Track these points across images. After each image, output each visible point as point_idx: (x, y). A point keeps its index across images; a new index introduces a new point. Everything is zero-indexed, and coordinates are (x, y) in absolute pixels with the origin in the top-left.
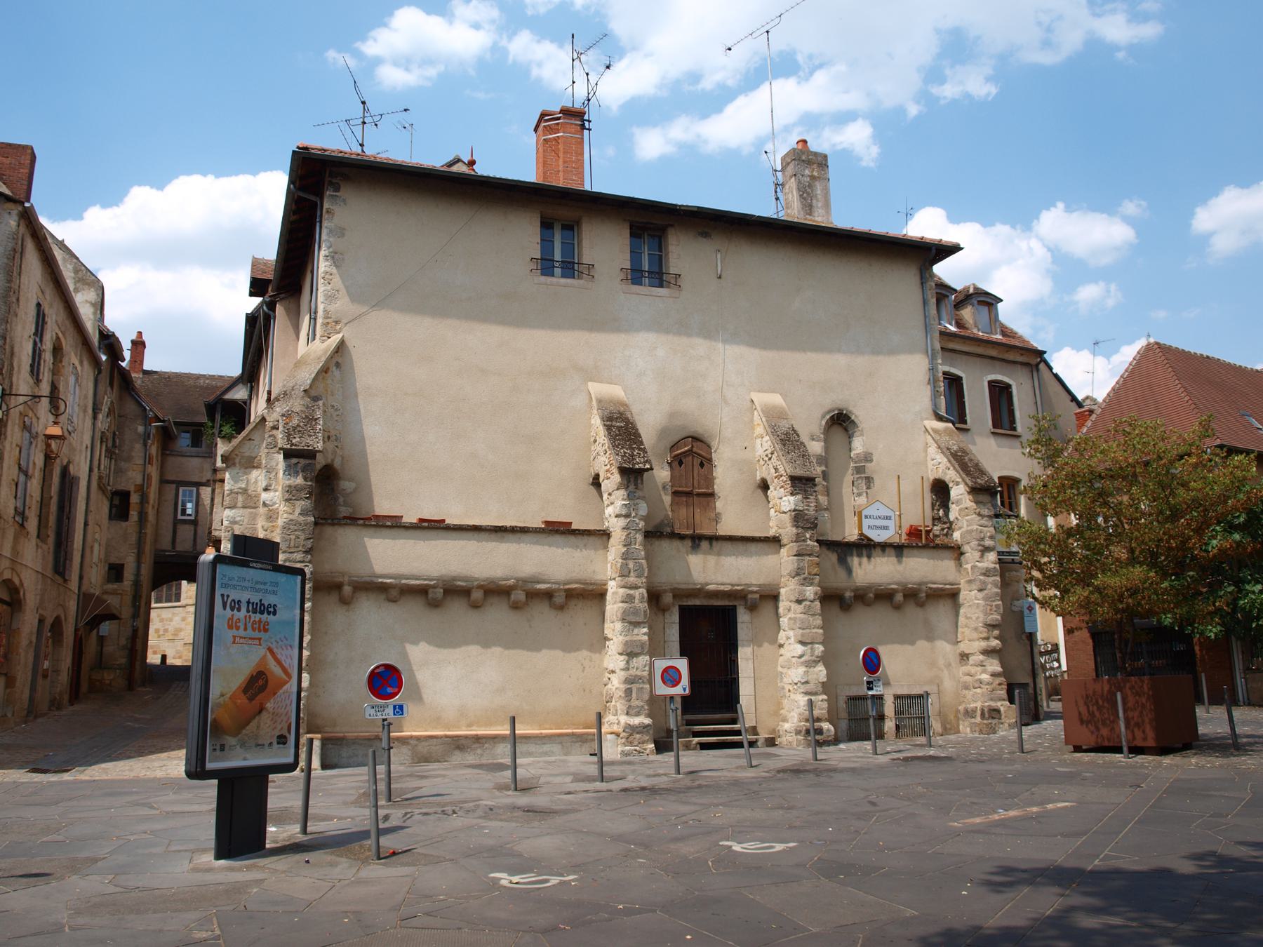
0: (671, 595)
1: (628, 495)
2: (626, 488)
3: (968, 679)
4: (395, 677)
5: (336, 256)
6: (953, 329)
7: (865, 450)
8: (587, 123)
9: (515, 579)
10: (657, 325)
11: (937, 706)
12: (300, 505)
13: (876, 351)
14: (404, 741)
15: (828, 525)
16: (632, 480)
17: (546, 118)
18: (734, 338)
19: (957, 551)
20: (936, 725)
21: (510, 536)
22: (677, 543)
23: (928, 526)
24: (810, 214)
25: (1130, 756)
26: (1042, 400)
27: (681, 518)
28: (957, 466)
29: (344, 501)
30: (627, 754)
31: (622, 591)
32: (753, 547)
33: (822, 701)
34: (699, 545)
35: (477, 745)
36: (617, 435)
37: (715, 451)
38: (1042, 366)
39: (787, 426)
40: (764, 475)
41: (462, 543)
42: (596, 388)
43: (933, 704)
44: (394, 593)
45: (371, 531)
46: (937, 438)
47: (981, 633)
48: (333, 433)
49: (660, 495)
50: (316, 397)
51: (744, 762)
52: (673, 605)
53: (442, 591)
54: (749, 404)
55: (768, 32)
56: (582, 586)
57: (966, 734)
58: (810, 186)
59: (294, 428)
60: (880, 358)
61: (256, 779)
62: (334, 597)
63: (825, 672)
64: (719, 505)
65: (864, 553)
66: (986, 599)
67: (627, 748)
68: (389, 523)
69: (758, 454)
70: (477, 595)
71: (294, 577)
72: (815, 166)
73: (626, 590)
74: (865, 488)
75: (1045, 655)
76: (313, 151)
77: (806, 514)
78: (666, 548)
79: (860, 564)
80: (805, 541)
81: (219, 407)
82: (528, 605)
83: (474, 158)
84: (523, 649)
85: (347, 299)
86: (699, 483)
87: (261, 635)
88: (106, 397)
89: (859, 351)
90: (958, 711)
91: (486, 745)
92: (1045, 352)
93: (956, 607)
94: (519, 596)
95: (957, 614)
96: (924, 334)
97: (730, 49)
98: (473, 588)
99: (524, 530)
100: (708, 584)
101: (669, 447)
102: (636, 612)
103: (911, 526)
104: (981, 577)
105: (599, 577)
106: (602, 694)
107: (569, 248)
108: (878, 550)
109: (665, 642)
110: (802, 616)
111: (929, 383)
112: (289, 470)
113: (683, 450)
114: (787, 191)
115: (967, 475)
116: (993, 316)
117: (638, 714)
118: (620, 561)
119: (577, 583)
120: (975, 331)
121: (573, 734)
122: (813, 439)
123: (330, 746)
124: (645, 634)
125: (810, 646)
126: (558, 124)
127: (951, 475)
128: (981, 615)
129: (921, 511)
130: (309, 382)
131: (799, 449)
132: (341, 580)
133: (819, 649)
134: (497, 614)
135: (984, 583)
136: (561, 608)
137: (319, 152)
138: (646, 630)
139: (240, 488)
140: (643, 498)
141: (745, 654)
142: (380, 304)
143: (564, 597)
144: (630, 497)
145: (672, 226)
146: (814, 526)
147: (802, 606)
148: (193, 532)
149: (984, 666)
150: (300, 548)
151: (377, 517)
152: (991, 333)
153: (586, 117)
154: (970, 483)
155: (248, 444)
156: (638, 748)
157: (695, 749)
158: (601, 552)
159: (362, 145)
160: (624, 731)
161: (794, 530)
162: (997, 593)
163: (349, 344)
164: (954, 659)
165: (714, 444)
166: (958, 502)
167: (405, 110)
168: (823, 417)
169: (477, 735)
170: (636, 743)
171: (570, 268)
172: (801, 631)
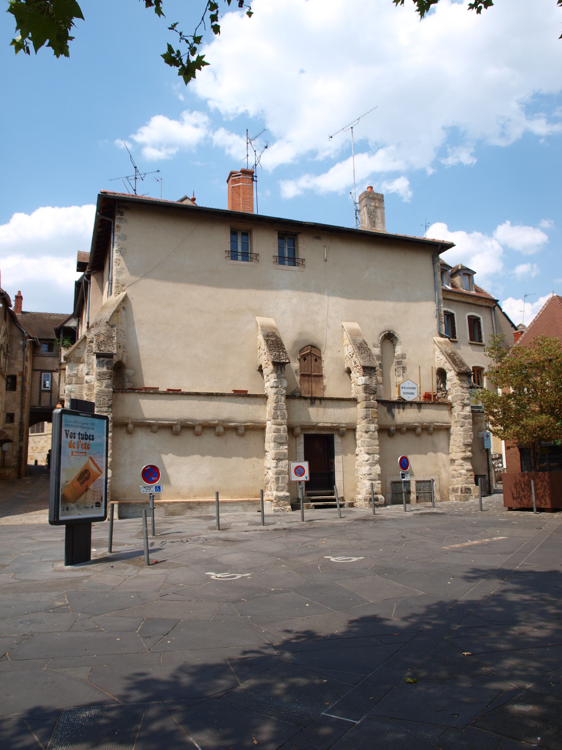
0: (300, 428)
1: (277, 376)
2: (276, 373)
3: (454, 472)
4: (156, 472)
5: (122, 250)
6: (449, 288)
7: (402, 353)
8: (255, 178)
9: (218, 420)
10: (293, 286)
11: (438, 487)
12: (105, 382)
13: (409, 300)
14: (161, 504)
15: (382, 392)
16: (279, 368)
17: (233, 175)
18: (333, 293)
19: (450, 406)
20: (437, 496)
21: (216, 398)
22: (303, 402)
23: (435, 393)
24: (374, 227)
25: (537, 513)
26: (497, 326)
27: (305, 388)
28: (450, 361)
29: (128, 380)
30: (277, 511)
31: (274, 426)
32: (342, 403)
33: (378, 484)
34: (314, 403)
35: (199, 507)
36: (271, 345)
37: (323, 353)
38: (496, 308)
39: (361, 340)
40: (349, 366)
41: (190, 402)
42: (260, 320)
43: (436, 486)
44: (155, 428)
45: (143, 396)
46: (440, 346)
47: (461, 449)
48: (122, 344)
49: (294, 376)
50: (113, 325)
51: (337, 515)
52: (301, 433)
53: (180, 427)
54: (341, 328)
55: (352, 128)
56: (253, 424)
57: (453, 501)
58: (374, 211)
59: (101, 342)
60: (411, 304)
61: (86, 524)
62: (124, 430)
63: (380, 469)
64: (325, 381)
65: (401, 406)
66: (464, 431)
67: (277, 508)
68: (152, 392)
69: (345, 354)
70: (198, 429)
71: (103, 420)
72: (377, 201)
73: (276, 426)
74: (402, 372)
75: (495, 460)
76: (109, 194)
77: (371, 386)
78: (297, 403)
79: (399, 413)
80: (370, 400)
81: (62, 331)
82: (225, 434)
83: (195, 197)
84: (223, 457)
85: (128, 273)
86: (315, 370)
87: (87, 451)
88: (3, 326)
89: (399, 300)
90: (449, 489)
91: (204, 507)
92: (498, 301)
93: (449, 435)
94: (220, 429)
95: (449, 439)
96: (434, 291)
97: (331, 137)
98: (196, 425)
99: (222, 395)
100: (319, 423)
101: (299, 350)
102: (281, 437)
103: (426, 393)
104: (462, 420)
105: (262, 419)
106: (263, 480)
107: (246, 245)
108: (408, 405)
109: (296, 453)
110: (368, 439)
111: (436, 317)
112: (99, 364)
113: (306, 352)
114: (362, 214)
115: (456, 366)
116: (471, 281)
117: (282, 491)
118: (273, 411)
119: (250, 422)
120: (461, 289)
121: (249, 501)
122: (375, 347)
123: (123, 507)
124: (286, 449)
125: (372, 455)
126: (239, 178)
127: (447, 366)
128: (462, 440)
129: (432, 384)
130: (109, 317)
131: (367, 352)
132: (127, 421)
133: (377, 457)
134: (209, 439)
135: (463, 422)
136: (242, 435)
137: (112, 195)
138: (286, 447)
139: (74, 374)
140: (285, 378)
141: (338, 459)
142: (146, 275)
143: (244, 430)
144: (278, 377)
145: (300, 233)
146: (375, 393)
147: (368, 434)
148: (49, 397)
149: (463, 466)
150: (106, 405)
151: (146, 388)
152: (470, 290)
153: (254, 175)
154: (457, 370)
155: (77, 351)
156: (282, 508)
157: (312, 508)
158: (263, 406)
159: (135, 190)
160: (275, 499)
161: (364, 395)
162: (470, 428)
163: (130, 297)
164: (447, 462)
165: (323, 349)
166: (451, 380)
167: (158, 171)
168: (380, 335)
169: (199, 501)
170: (281, 505)
171: (246, 256)
172: (368, 447)
